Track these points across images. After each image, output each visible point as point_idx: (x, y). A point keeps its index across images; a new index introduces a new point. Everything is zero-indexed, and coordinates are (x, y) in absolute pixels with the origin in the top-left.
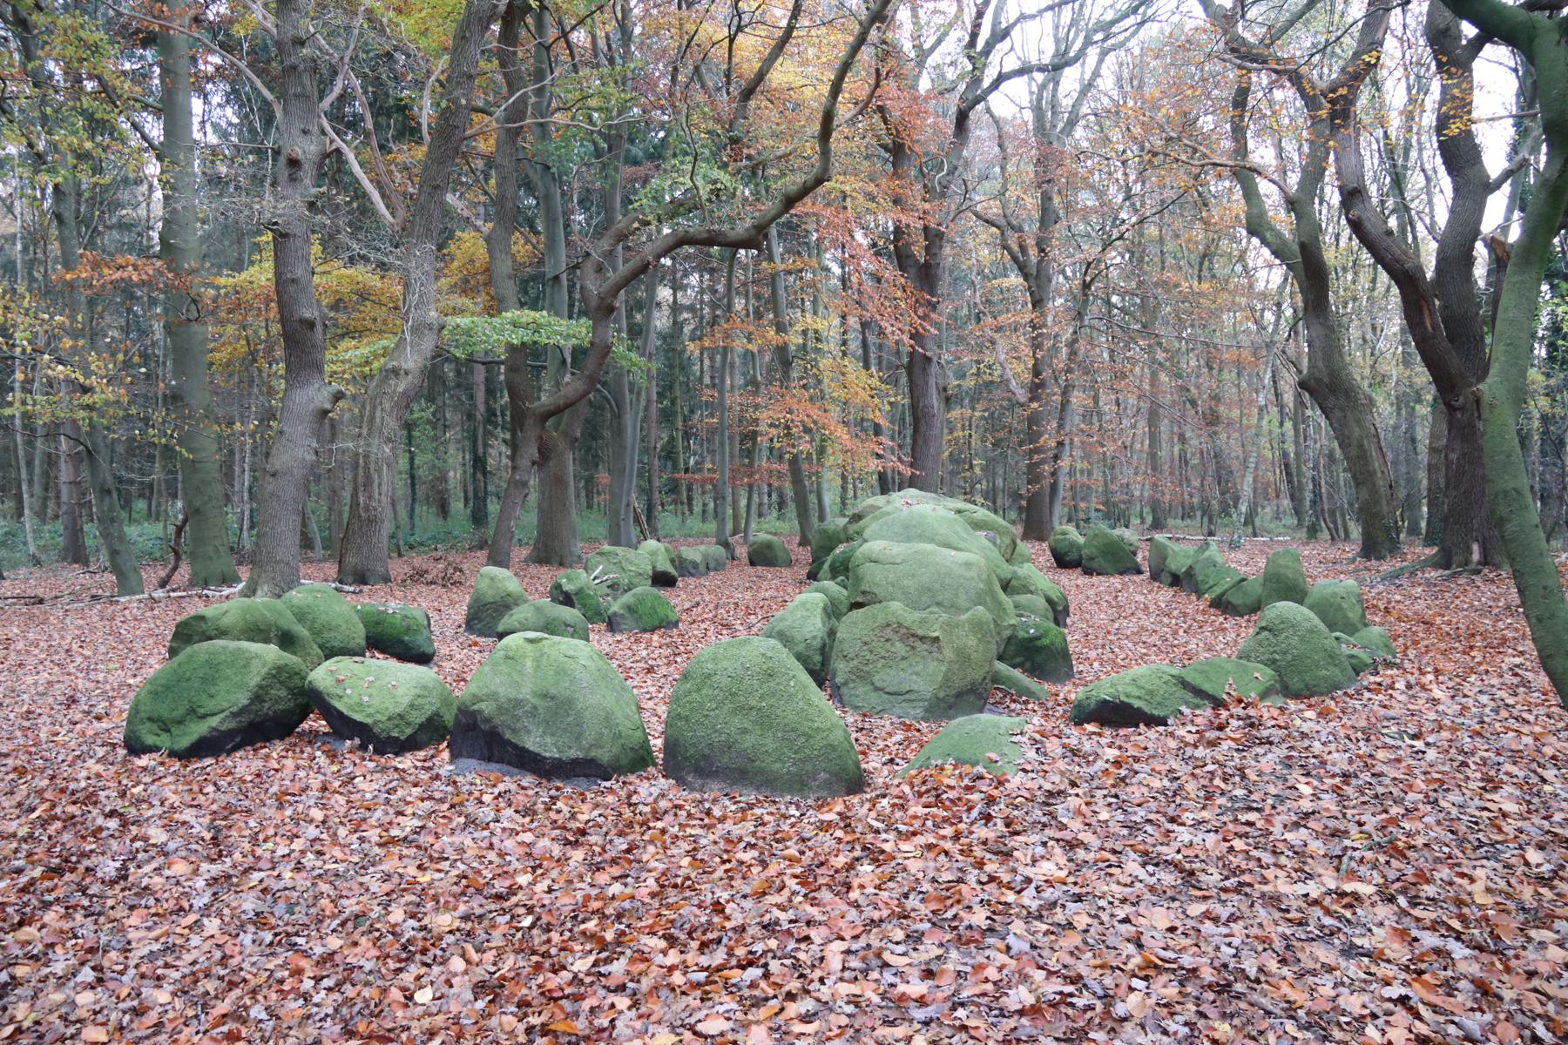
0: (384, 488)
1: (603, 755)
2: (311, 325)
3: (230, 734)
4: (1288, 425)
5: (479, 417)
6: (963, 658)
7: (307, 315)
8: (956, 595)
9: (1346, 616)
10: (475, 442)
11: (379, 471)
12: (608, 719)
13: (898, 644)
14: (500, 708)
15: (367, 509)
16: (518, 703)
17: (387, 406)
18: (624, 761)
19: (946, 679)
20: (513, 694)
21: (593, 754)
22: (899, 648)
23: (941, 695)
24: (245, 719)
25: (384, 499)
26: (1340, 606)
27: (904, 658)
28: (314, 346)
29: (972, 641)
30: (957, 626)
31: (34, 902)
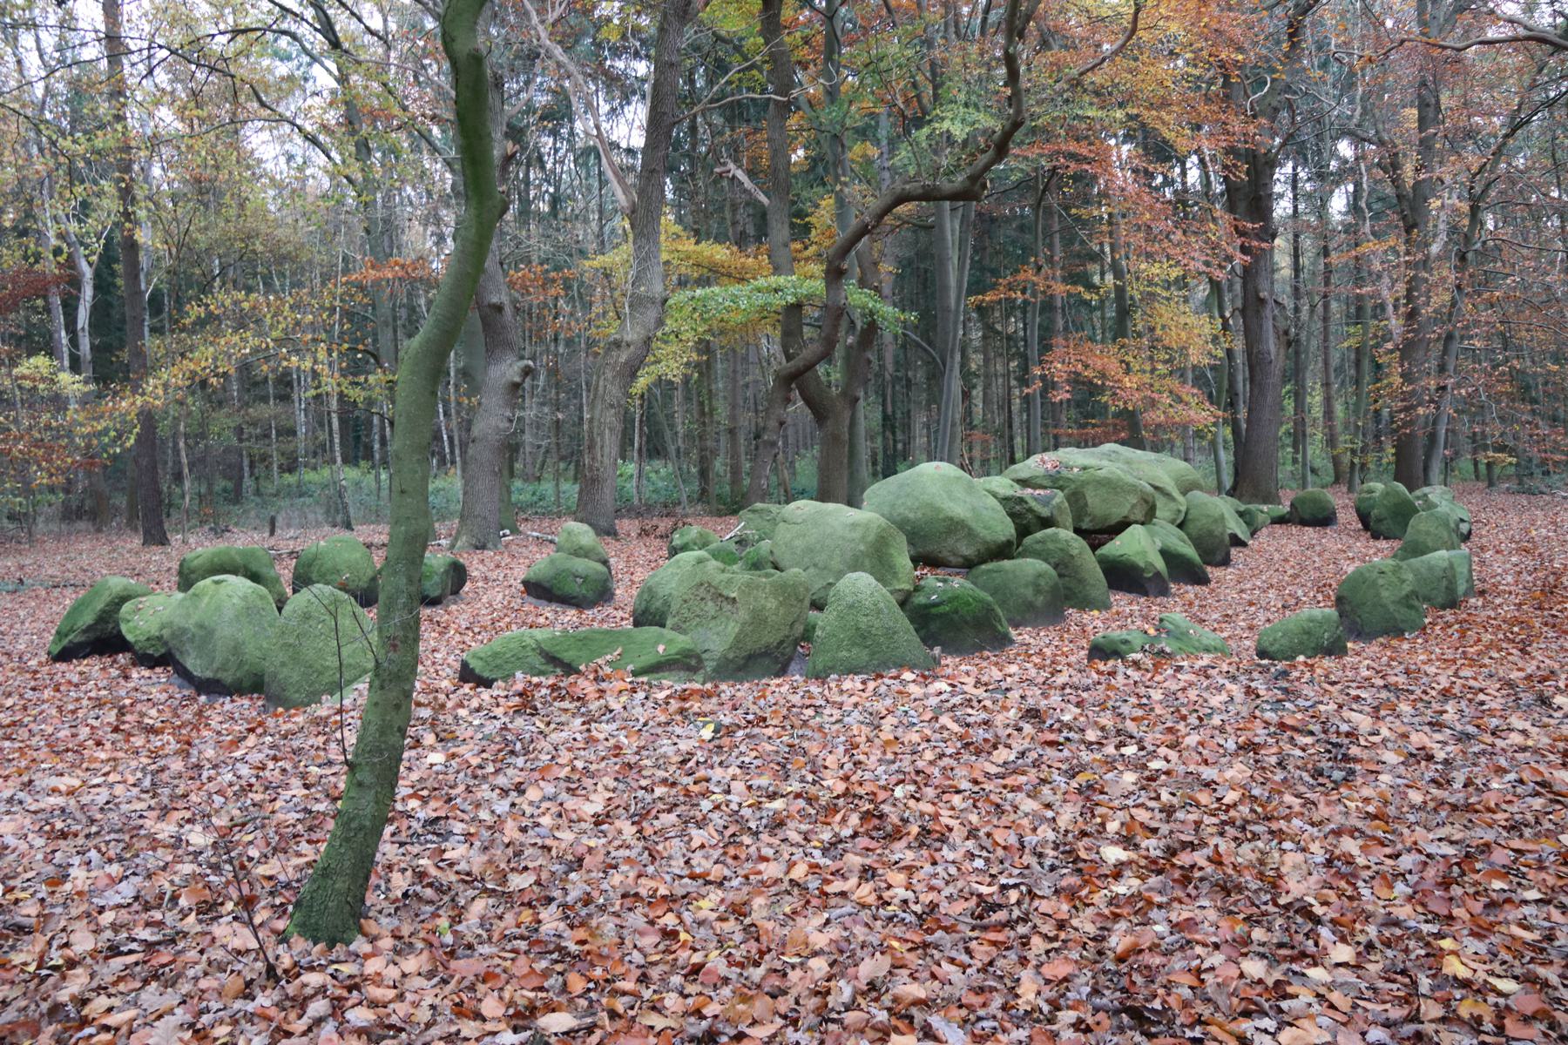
0: (607, 450)
1: (228, 677)
2: (499, 308)
3: (80, 646)
4: (587, 416)
5: (888, 377)
6: (758, 619)
7: (495, 300)
8: (831, 558)
9: (1378, 595)
10: (884, 401)
11: (601, 434)
12: (236, 649)
13: (710, 604)
14: (173, 634)
15: (591, 469)
16: (184, 631)
17: (609, 375)
18: (246, 684)
19: (737, 639)
20: (183, 624)
21: (219, 675)
22: (710, 607)
23: (731, 656)
24: (92, 636)
25: (606, 460)
26: (1374, 583)
27: (714, 618)
28: (504, 327)
29: (772, 604)
30: (757, 587)
31: (752, 850)
